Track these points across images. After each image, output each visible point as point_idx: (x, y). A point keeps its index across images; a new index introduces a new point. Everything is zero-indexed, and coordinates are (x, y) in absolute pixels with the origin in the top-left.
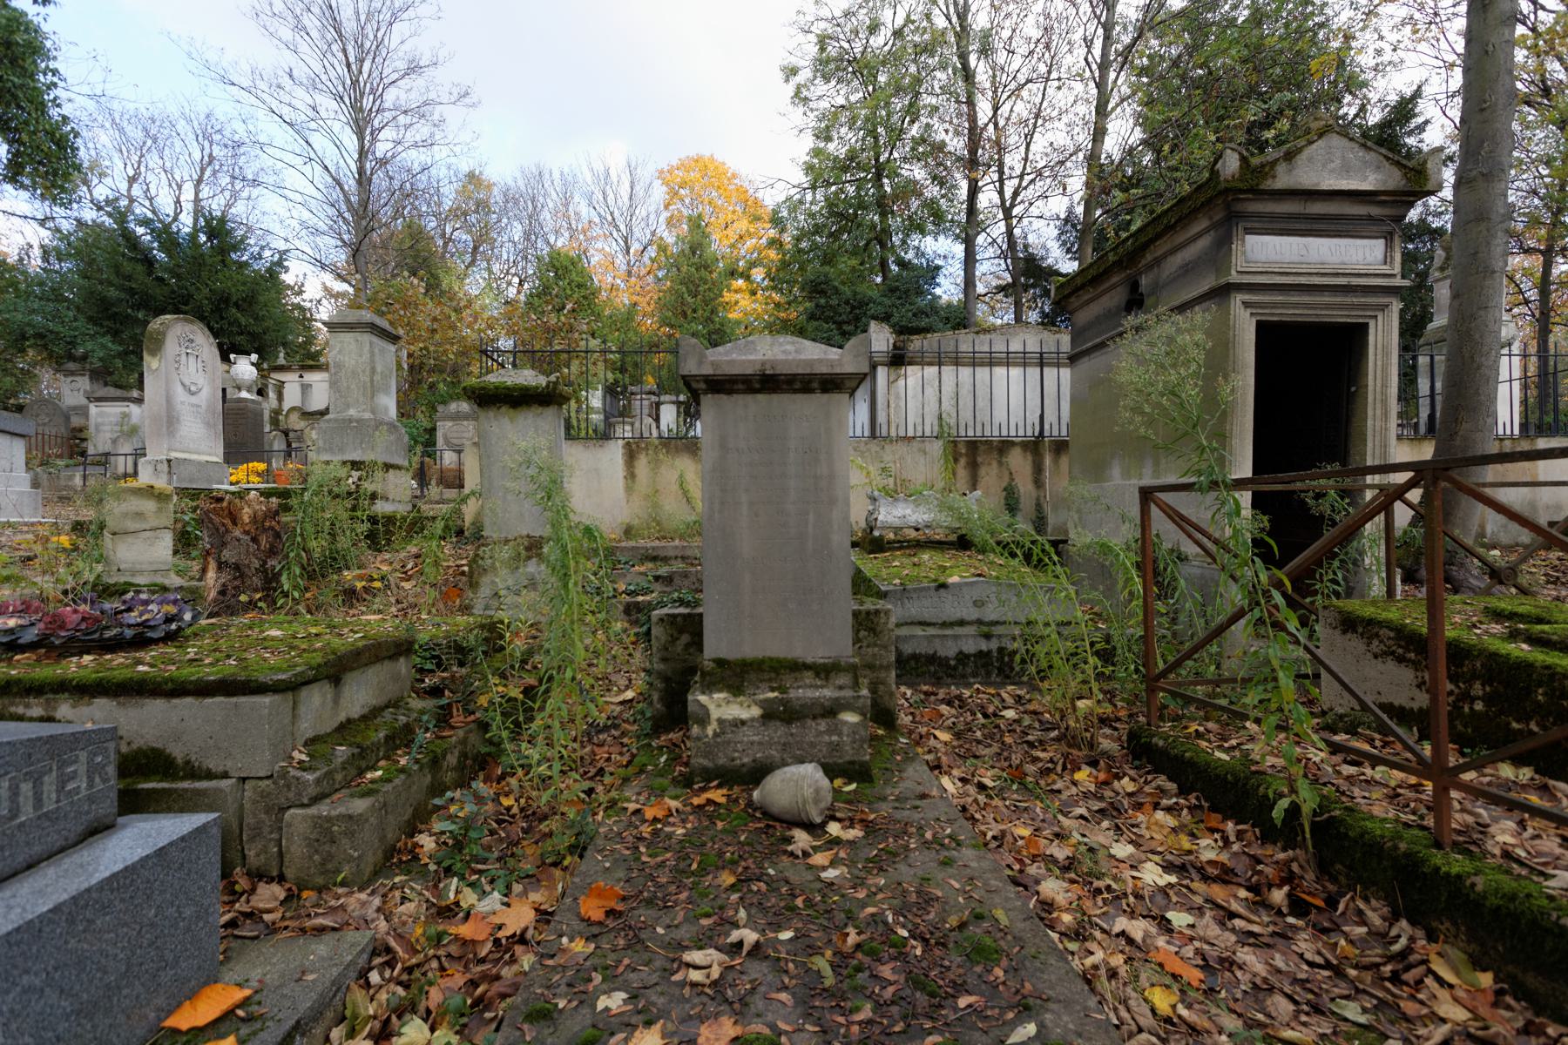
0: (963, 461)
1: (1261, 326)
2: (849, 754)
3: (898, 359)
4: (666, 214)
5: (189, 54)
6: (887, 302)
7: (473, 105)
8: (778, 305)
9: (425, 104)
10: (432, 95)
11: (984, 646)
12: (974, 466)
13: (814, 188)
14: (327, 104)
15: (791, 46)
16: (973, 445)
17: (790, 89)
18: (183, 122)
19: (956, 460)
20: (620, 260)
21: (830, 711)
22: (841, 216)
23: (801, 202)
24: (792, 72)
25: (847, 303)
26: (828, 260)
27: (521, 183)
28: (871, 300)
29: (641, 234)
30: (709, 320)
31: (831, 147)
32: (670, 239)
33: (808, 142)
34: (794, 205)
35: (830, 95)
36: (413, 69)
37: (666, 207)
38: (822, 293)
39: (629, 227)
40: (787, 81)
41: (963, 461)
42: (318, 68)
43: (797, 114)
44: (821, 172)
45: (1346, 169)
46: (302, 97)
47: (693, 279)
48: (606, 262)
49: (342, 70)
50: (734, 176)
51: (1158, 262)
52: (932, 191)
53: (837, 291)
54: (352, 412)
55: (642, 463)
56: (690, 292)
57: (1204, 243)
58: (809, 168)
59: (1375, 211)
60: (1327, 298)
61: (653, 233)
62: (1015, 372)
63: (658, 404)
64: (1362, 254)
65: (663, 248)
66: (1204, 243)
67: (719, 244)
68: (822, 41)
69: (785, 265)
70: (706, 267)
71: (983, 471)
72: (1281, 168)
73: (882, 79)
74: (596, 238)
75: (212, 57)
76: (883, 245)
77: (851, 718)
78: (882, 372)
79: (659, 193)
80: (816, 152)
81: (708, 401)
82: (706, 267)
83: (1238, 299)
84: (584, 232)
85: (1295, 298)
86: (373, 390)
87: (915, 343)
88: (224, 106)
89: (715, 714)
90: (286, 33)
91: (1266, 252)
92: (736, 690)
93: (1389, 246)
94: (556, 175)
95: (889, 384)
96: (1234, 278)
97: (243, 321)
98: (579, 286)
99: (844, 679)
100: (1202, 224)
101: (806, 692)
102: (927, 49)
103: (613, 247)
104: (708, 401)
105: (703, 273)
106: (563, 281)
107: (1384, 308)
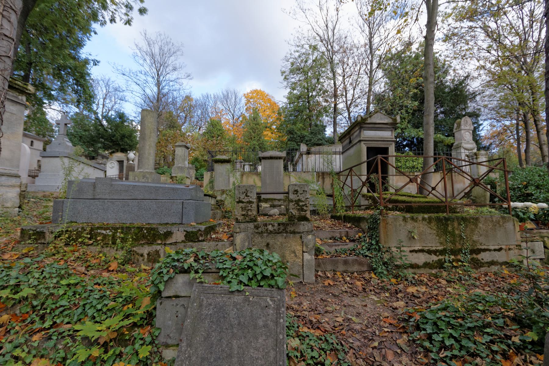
0: (321, 177)
1: (368, 148)
2: (283, 212)
3: (308, 153)
4: (246, 107)
5: (113, 67)
6: (310, 136)
7: (191, 79)
8: (279, 136)
9: (177, 78)
10: (180, 76)
11: (314, 209)
12: (323, 178)
13: (290, 104)
14: (150, 79)
15: (283, 65)
16: (323, 174)
17: (283, 77)
18: (101, 82)
19: (319, 177)
20: (231, 121)
21: (280, 206)
22: (299, 111)
23: (286, 108)
24: (283, 73)
25: (299, 136)
26: (294, 124)
27: (202, 99)
28: (306, 136)
29: (238, 113)
30: (259, 140)
31: (295, 92)
32: (247, 115)
33: (289, 90)
34: (284, 109)
35: (295, 78)
36: (175, 69)
37: (246, 105)
38: (292, 134)
39: (234, 111)
40: (282, 75)
41: (321, 177)
42: (148, 70)
43: (285, 83)
44: (292, 98)
45: (381, 119)
46: (143, 77)
47: (254, 126)
48: (226, 119)
49: (155, 71)
50: (267, 95)
51: (353, 134)
52: (324, 104)
53: (296, 133)
54: (180, 165)
55: (244, 177)
56: (253, 132)
57: (358, 131)
58: (288, 98)
59: (388, 126)
60: (380, 142)
61: (241, 113)
62: (338, 156)
63: (244, 165)
64: (387, 134)
65: (244, 117)
66: (358, 131)
67: (262, 119)
68: (292, 64)
69: (281, 125)
70: (258, 124)
71: (325, 180)
72: (369, 119)
73: (309, 74)
74: (223, 115)
75: (119, 68)
76: (310, 120)
77: (283, 207)
78: (304, 156)
79: (244, 101)
80: (290, 93)
81: (262, 160)
82: (258, 124)
83: (362, 143)
84: (220, 113)
85: (374, 142)
86: (184, 160)
87: (313, 149)
88: (120, 81)
90: (141, 62)
91: (368, 134)
92: (266, 202)
93: (392, 133)
94: (212, 96)
95: (307, 159)
96: (362, 139)
97: (128, 142)
98: (219, 130)
99: (282, 201)
100: (357, 128)
101: (276, 203)
102: (322, 65)
103: (229, 117)
104: (262, 160)
105: (257, 126)
106: (215, 130)
107: (391, 144)
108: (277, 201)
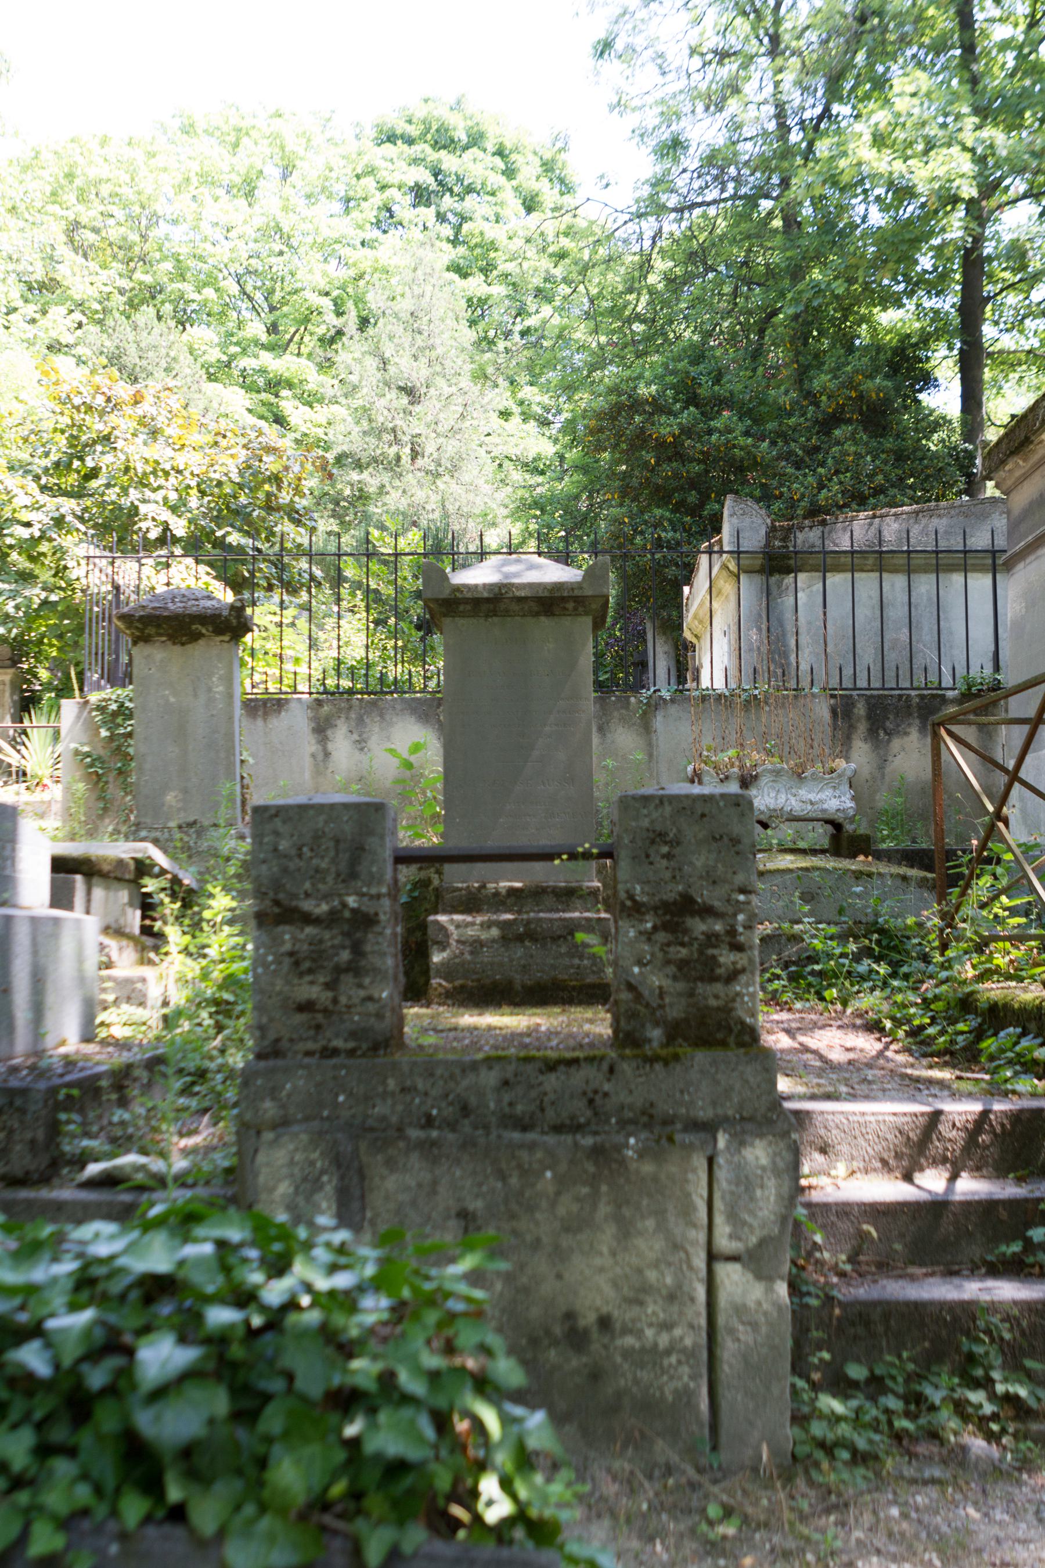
89: (455, 934)
108: (549, 900)
